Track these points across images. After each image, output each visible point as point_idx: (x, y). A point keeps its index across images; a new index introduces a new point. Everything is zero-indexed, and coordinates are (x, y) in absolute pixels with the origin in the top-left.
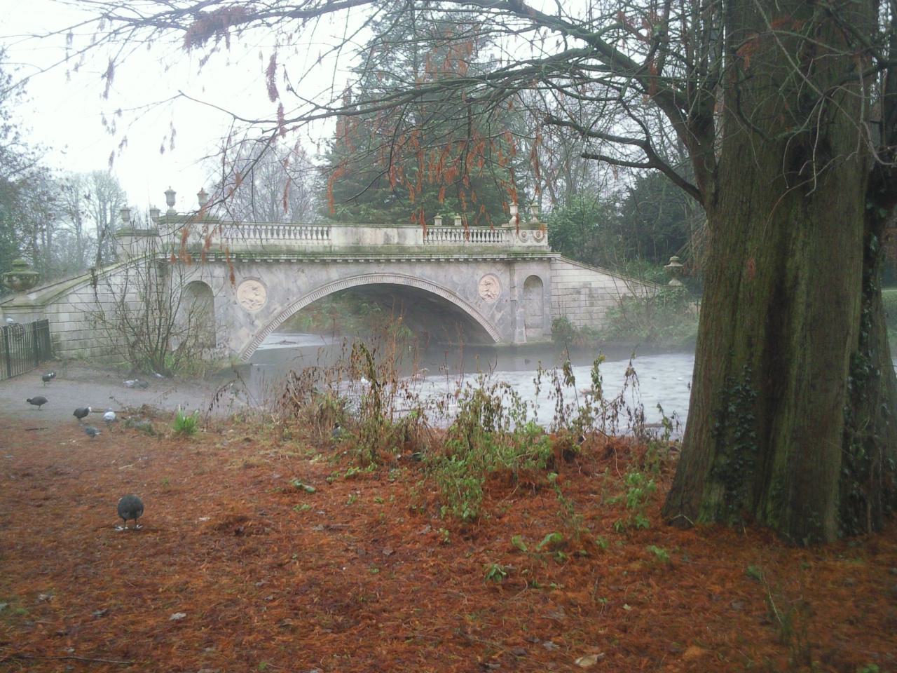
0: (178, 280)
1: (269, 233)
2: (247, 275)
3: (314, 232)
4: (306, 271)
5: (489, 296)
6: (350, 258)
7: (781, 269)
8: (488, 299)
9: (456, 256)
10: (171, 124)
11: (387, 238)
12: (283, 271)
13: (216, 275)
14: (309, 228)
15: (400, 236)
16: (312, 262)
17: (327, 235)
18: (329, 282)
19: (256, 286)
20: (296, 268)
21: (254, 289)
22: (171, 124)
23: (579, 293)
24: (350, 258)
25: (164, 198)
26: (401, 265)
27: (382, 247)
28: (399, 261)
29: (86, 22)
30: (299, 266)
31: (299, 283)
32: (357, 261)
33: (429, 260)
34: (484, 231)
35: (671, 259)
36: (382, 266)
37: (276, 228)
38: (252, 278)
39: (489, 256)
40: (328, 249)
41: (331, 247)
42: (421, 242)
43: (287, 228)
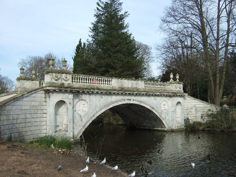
31: (100, 102)
42: (143, 87)
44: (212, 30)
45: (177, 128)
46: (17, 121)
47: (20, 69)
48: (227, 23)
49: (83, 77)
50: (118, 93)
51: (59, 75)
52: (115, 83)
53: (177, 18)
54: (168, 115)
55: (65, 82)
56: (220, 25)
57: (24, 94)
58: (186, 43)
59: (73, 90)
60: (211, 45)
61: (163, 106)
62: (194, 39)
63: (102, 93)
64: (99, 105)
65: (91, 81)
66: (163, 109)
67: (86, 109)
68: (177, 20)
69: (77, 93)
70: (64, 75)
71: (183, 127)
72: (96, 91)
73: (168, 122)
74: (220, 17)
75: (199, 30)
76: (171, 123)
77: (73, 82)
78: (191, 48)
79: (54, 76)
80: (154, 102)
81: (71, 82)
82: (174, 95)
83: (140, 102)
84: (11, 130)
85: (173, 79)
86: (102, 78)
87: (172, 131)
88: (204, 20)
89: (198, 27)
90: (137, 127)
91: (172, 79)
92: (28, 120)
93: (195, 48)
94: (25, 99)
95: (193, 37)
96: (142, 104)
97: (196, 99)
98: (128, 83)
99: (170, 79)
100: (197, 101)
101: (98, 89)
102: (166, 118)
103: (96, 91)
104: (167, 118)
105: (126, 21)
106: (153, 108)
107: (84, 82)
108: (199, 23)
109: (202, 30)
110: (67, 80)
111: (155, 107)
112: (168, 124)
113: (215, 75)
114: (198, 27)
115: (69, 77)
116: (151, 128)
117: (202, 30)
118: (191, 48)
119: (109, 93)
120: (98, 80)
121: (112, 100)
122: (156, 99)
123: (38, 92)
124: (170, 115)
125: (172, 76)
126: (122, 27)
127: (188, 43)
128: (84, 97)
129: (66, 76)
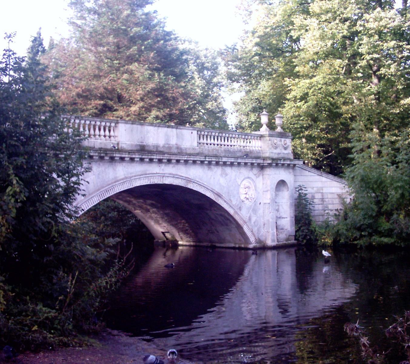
1: (87, 129)
5: (247, 199)
7: (222, 198)
8: (247, 202)
9: (224, 160)
10: (40, 28)
11: (167, 137)
14: (243, 137)
15: (178, 136)
16: (102, 158)
22: (40, 28)
24: (137, 156)
26: (124, 164)
27: (164, 147)
32: (142, 160)
34: (98, 123)
36: (163, 166)
37: (98, 123)
39: (249, 161)
41: (118, 144)
42: (195, 144)
43: (108, 124)
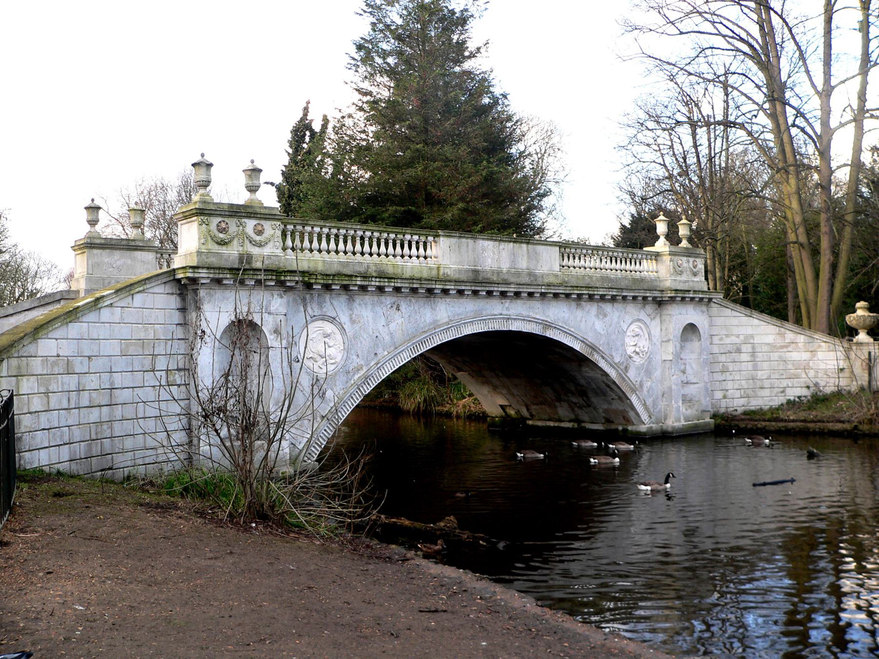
0: (217, 312)
2: (317, 312)
3: (375, 240)
4: (403, 307)
5: (638, 353)
6: (468, 288)
12: (369, 307)
13: (271, 309)
17: (425, 250)
18: (435, 325)
19: (329, 331)
20: (388, 300)
21: (327, 336)
23: (739, 351)
25: (242, 180)
28: (531, 295)
29: (843, 82)
30: (394, 299)
31: (392, 326)
32: (475, 293)
33: (568, 296)
35: (858, 305)
36: (507, 303)
38: (324, 318)
40: (434, 273)
42: (557, 268)
44: (802, 57)
45: (683, 423)
46: (111, 428)
47: (86, 208)
48: (859, 35)
49: (326, 230)
50: (624, 298)
51: (232, 225)
52: (445, 254)
53: (673, 16)
54: (649, 373)
55: (255, 251)
56: (796, 48)
57: (103, 297)
58: (706, 110)
59: (288, 278)
60: (803, 115)
61: (630, 341)
62: (735, 93)
63: (397, 290)
64: (387, 338)
65: (371, 247)
66: (630, 350)
67: (336, 352)
68: (672, 23)
69: (307, 285)
70: (250, 224)
71: (708, 420)
72: (373, 283)
73: (649, 402)
74: (835, 9)
75: (755, 57)
76: (662, 405)
77: (284, 249)
78: (727, 124)
79: (213, 227)
80: (599, 325)
81: (279, 252)
82: (659, 300)
83: (547, 325)
84: (59, 433)
85: (667, 237)
86: (381, 232)
87: (663, 438)
88: (776, 20)
89: (751, 46)
90: (530, 422)
91: (662, 239)
92: (123, 396)
93: (742, 126)
94: (105, 314)
95: (732, 87)
96: (550, 334)
97: (756, 314)
98: (494, 255)
99: (658, 237)
100: (756, 322)
101: (382, 275)
102: (641, 386)
103: (377, 284)
104: (647, 384)
105: (475, 35)
106: (593, 348)
107: (362, 254)
108: (755, 30)
109: (765, 57)
110: (270, 247)
111: (600, 344)
112: (650, 407)
113: (812, 228)
114: (751, 46)
115: (271, 229)
116: (583, 424)
117: (765, 57)
118: (727, 124)
119: (428, 289)
120: (375, 240)
121: (438, 318)
122: (605, 316)
123: (151, 291)
124: (657, 374)
125: (661, 228)
126: (459, 52)
127: (713, 104)
128: (337, 306)
129: (260, 228)
